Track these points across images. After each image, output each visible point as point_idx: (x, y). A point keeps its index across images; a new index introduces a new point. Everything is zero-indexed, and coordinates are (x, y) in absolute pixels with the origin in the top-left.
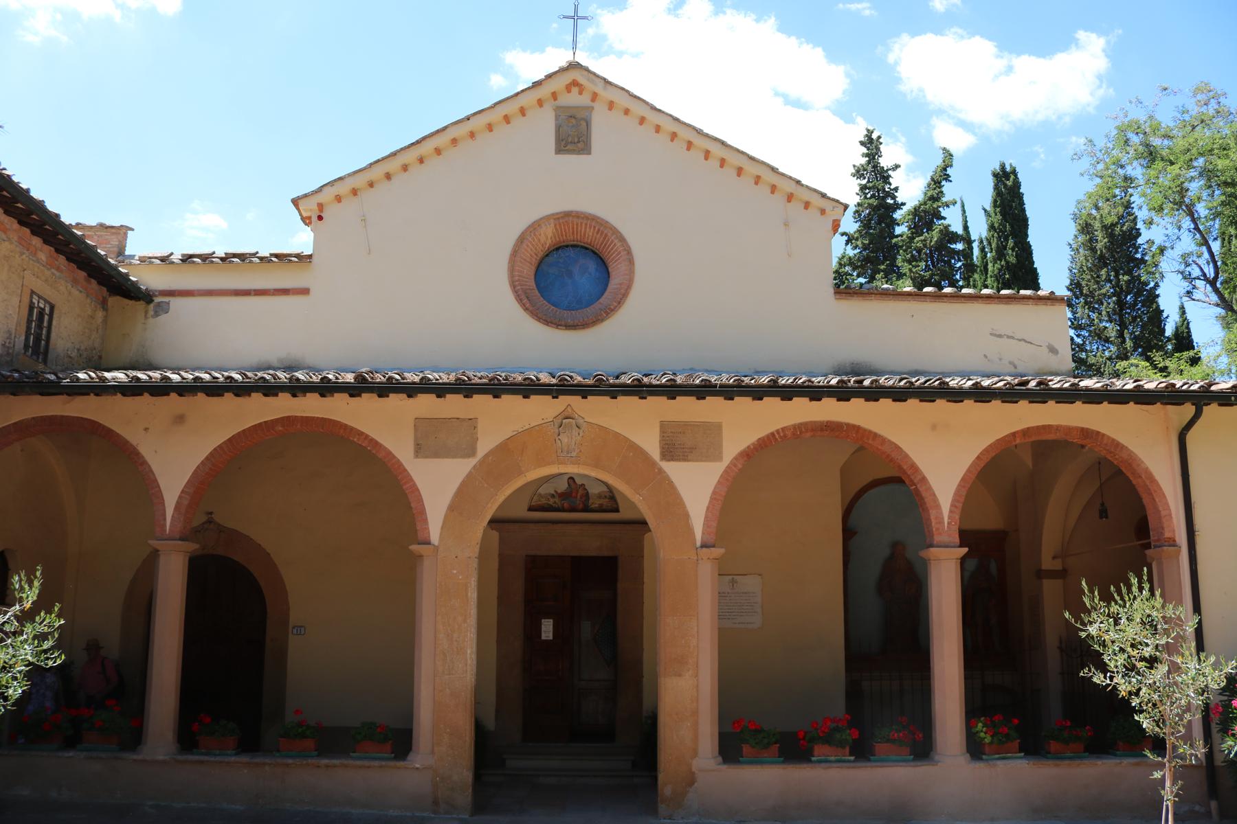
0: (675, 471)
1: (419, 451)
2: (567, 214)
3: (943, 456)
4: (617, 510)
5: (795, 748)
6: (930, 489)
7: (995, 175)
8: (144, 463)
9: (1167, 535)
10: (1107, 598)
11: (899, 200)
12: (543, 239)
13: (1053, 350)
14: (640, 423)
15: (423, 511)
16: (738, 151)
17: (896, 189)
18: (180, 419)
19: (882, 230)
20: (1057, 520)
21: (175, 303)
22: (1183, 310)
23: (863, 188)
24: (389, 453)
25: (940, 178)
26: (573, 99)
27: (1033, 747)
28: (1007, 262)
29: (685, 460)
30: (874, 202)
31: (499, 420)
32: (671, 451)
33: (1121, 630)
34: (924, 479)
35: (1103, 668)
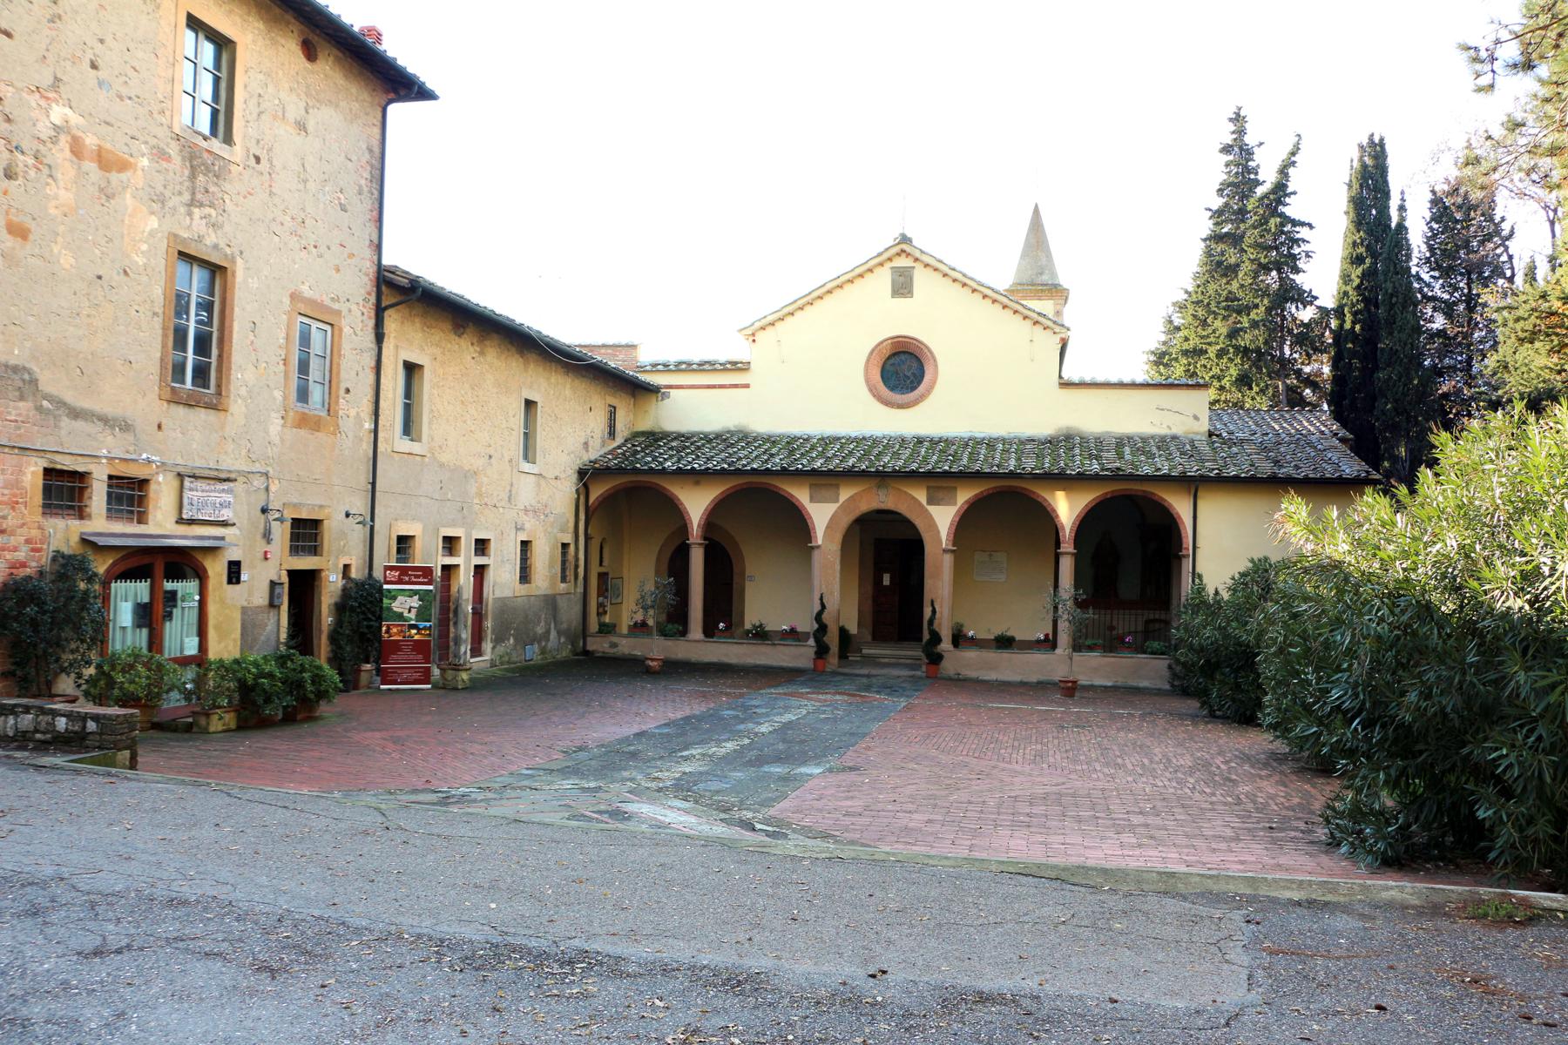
1: (812, 500)
13: (1196, 418)
26: (903, 262)
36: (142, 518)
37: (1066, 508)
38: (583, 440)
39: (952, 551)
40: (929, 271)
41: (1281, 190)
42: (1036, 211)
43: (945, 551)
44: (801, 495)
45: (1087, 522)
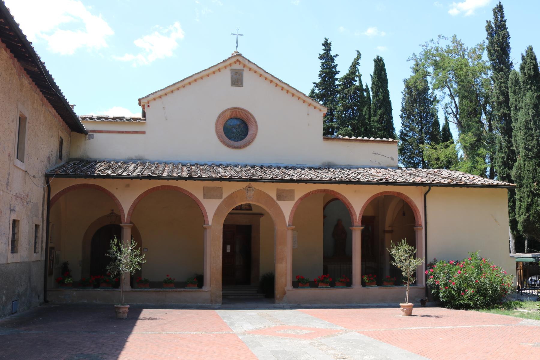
0: (280, 203)
1: (205, 197)
2: (235, 108)
3: (358, 202)
4: (251, 210)
5: (314, 284)
6: (353, 209)
7: (375, 61)
8: (116, 199)
9: (420, 223)
10: (397, 245)
11: (338, 70)
12: (226, 116)
13: (392, 159)
14: (271, 190)
15: (206, 215)
16: (293, 88)
17: (337, 65)
18: (128, 186)
19: (330, 83)
20: (390, 217)
21: (96, 135)
22: (446, 119)
23: (323, 64)
24: (196, 197)
25: (355, 64)
26: (237, 67)
27: (380, 283)
28: (379, 99)
29: (284, 200)
30: (327, 70)
31: (229, 189)
32: (279, 198)
33: (400, 253)
34: (352, 207)
35: (395, 261)
38: (48, 155)
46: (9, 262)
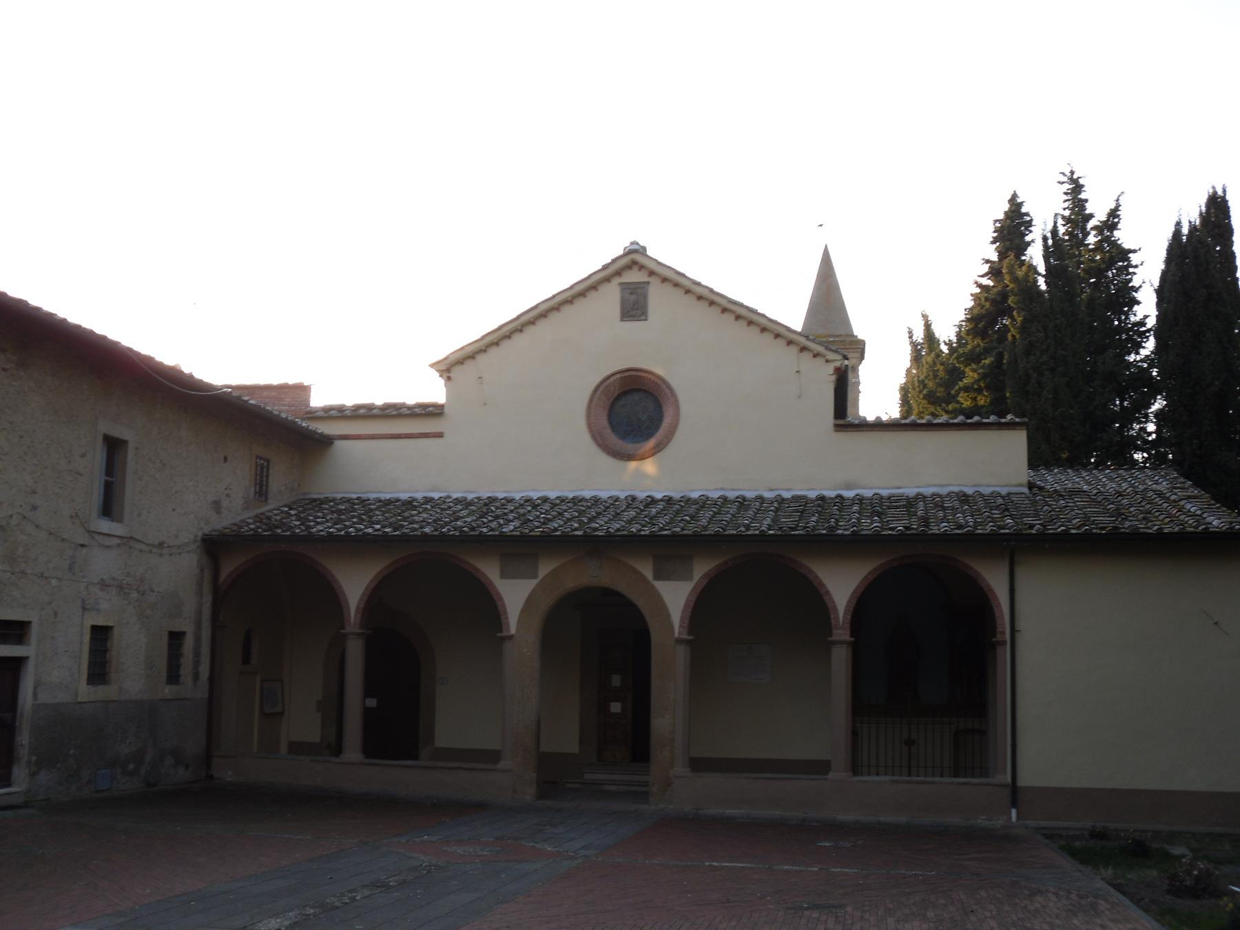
0: (659, 585)
1: (504, 575)
6: (831, 598)
26: (633, 277)
34: (828, 592)
36: (183, 633)
37: (841, 585)
39: (688, 642)
40: (667, 287)
41: (1112, 222)
42: (826, 262)
43: (679, 641)
44: (490, 570)
45: (863, 603)
46: (79, 700)
